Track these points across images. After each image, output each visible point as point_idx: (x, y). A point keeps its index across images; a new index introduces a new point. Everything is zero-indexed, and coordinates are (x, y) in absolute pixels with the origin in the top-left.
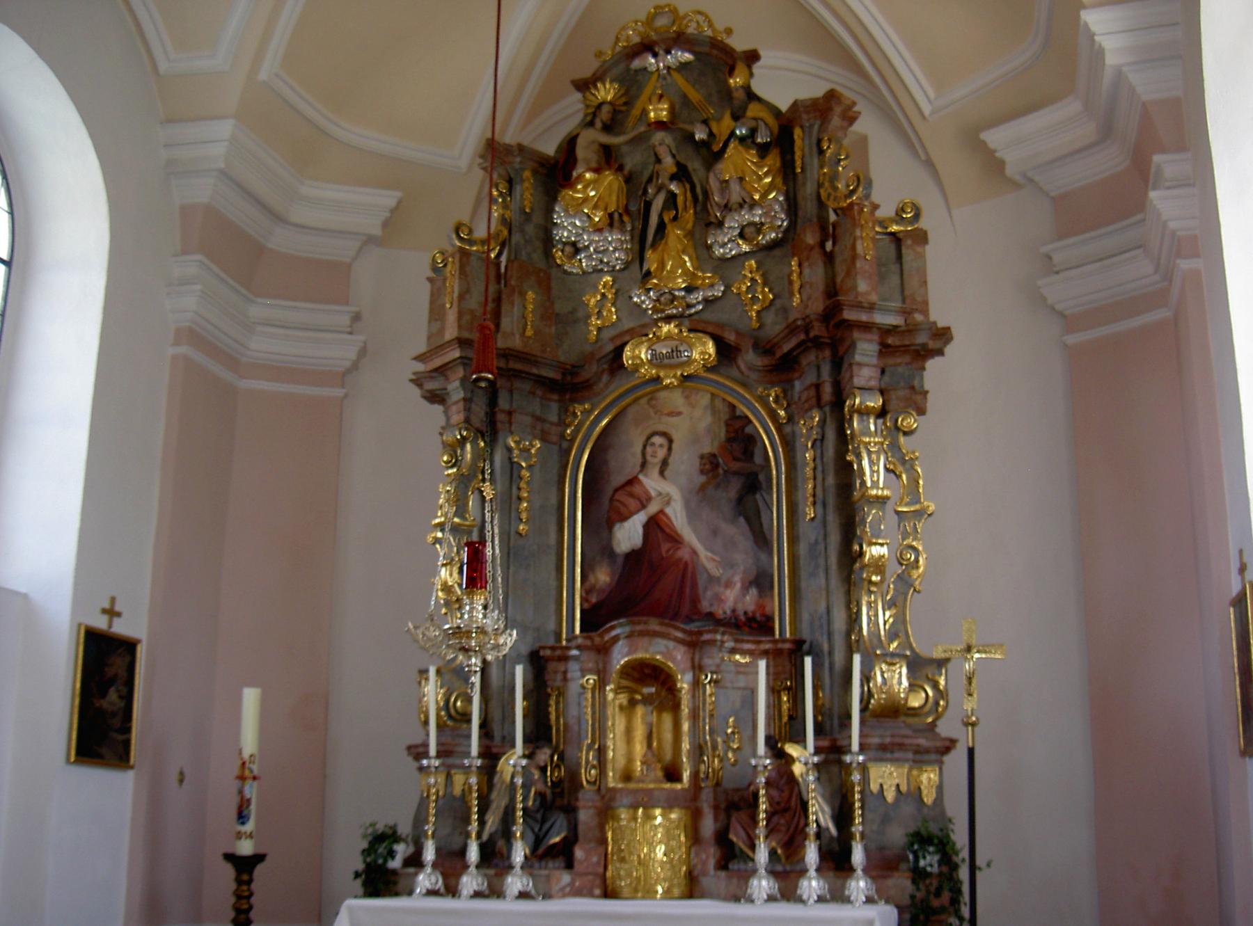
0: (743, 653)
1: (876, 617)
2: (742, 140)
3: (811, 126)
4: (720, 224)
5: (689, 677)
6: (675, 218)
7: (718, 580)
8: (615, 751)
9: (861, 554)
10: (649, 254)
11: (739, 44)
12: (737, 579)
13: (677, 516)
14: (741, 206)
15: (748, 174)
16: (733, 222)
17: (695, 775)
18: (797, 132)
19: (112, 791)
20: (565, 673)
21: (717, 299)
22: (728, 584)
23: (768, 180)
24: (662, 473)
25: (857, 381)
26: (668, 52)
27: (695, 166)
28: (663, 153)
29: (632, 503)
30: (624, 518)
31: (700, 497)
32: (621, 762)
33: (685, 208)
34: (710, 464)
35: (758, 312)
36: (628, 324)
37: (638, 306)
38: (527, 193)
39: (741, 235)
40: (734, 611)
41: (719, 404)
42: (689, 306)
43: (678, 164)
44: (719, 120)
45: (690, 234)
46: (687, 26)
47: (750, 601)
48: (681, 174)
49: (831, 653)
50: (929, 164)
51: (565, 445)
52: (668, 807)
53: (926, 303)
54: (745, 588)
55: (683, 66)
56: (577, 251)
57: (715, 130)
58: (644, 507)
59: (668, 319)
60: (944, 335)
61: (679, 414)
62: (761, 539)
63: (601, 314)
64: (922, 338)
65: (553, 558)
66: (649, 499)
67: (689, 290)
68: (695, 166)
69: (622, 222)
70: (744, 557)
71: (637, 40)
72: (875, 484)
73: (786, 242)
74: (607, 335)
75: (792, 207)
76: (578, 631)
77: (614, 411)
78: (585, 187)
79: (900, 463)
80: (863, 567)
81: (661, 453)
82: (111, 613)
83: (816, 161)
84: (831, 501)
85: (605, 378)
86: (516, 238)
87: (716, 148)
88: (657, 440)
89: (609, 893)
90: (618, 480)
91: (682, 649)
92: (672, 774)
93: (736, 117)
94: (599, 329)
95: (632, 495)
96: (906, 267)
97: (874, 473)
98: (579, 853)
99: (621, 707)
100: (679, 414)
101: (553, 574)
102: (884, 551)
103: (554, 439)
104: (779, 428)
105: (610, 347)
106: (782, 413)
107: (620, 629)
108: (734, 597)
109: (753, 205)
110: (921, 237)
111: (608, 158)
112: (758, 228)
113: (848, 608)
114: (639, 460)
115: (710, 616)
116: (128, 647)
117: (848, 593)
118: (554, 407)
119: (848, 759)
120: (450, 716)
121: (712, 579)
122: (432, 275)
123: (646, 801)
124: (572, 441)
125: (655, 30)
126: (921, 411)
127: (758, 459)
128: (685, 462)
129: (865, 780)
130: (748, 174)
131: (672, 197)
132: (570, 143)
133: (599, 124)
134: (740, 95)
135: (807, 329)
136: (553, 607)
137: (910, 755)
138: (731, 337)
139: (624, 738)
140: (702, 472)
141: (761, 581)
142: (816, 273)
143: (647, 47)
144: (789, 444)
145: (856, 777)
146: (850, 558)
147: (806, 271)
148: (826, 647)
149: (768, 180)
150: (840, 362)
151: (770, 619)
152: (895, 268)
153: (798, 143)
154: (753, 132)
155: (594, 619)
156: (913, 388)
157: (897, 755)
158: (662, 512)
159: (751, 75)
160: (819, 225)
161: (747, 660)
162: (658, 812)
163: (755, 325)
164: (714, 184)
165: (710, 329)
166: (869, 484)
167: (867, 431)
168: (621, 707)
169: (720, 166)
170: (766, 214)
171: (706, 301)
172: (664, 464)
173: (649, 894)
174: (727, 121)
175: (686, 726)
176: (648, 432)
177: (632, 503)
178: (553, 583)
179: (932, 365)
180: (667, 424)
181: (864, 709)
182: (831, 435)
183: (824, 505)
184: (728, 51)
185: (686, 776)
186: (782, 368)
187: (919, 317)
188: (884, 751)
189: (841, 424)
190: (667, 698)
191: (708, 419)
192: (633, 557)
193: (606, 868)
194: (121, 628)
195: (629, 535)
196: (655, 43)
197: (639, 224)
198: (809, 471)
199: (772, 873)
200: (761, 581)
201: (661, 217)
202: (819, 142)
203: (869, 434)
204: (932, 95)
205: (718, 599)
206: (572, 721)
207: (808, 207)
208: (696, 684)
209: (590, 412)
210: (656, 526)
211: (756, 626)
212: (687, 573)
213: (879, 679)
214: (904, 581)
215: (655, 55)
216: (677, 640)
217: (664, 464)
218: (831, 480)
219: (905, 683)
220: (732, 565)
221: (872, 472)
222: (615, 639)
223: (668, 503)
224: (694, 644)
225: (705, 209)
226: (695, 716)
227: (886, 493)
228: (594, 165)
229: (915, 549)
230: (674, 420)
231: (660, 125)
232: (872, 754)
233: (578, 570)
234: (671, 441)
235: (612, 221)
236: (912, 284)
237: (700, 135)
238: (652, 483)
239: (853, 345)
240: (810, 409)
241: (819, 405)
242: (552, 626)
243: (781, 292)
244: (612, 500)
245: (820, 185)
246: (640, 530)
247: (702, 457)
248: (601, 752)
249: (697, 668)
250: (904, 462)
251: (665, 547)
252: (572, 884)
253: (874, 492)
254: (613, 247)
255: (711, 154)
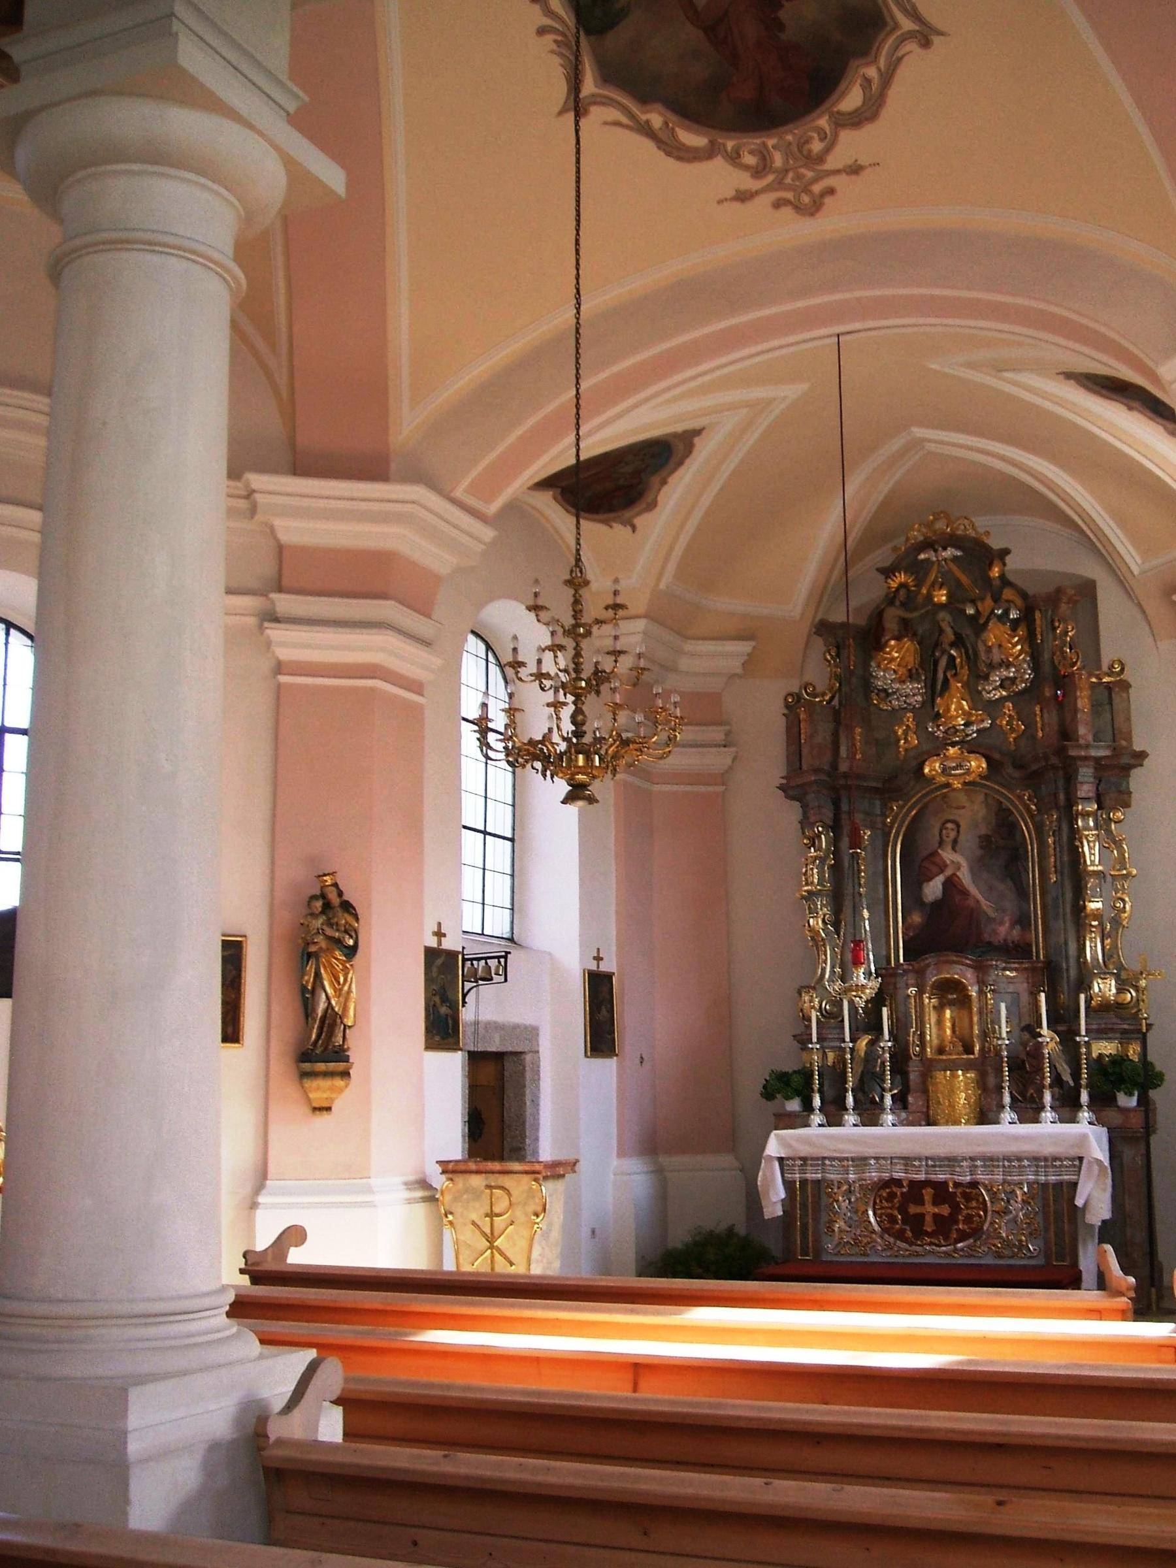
0: (1010, 970)
1: (1094, 949)
2: (1000, 617)
3: (1046, 611)
4: (986, 678)
5: (976, 988)
6: (956, 674)
7: (994, 920)
8: (931, 1034)
9: (1085, 907)
10: (938, 700)
11: (995, 543)
12: (1007, 919)
13: (965, 877)
14: (1000, 665)
15: (1005, 643)
16: (996, 678)
17: (982, 1049)
18: (1038, 615)
19: (608, 1067)
20: (895, 984)
21: (985, 729)
22: (1001, 923)
23: (1019, 647)
24: (954, 849)
25: (1081, 794)
26: (945, 549)
27: (967, 632)
28: (944, 625)
29: (935, 869)
30: (931, 879)
31: (979, 866)
32: (935, 1042)
33: (962, 667)
34: (986, 842)
35: (1015, 739)
36: (926, 747)
37: (933, 733)
38: (853, 657)
39: (1001, 686)
40: (1005, 940)
41: (990, 800)
42: (967, 735)
43: (956, 634)
44: (982, 599)
45: (966, 685)
46: (957, 529)
47: (1016, 933)
48: (958, 642)
49: (1068, 970)
50: (1140, 605)
51: (887, 830)
52: (966, 1070)
53: (1130, 733)
54: (1012, 926)
55: (955, 559)
56: (888, 695)
57: (980, 609)
58: (942, 871)
59: (953, 744)
60: (1141, 756)
61: (964, 807)
62: (1023, 893)
63: (907, 739)
64: (1125, 760)
65: (882, 907)
66: (946, 866)
67: (967, 725)
68: (967, 632)
69: (918, 674)
70: (1011, 904)
71: (921, 538)
72: (1092, 862)
73: (1033, 689)
74: (912, 754)
75: (1036, 666)
76: (901, 961)
77: (919, 806)
78: (892, 650)
79: (1111, 841)
80: (1086, 916)
81: (953, 834)
82: (598, 959)
83: (1051, 635)
84: (1066, 871)
85: (912, 783)
86: (845, 689)
87: (982, 621)
88: (949, 825)
89: (930, 1123)
90: (925, 853)
91: (970, 970)
92: (969, 1049)
93: (996, 600)
94: (906, 750)
95: (934, 863)
96: (1115, 707)
97: (1092, 855)
98: (910, 1099)
99: (934, 1007)
100: (964, 807)
101: (882, 915)
102: (1099, 905)
103: (880, 826)
104: (1032, 816)
105: (914, 763)
106: (1033, 807)
107: (930, 959)
108: (1004, 931)
109: (1008, 665)
110: (1125, 686)
111: (906, 629)
112: (1013, 680)
113: (1078, 941)
114: (938, 838)
115: (990, 943)
116: (609, 977)
117: (1078, 931)
118: (878, 803)
119: (1078, 1039)
120: (822, 1014)
121: (991, 920)
122: (786, 712)
123: (953, 1066)
124: (891, 828)
125: (935, 532)
126: (1126, 805)
127: (1018, 837)
128: (968, 840)
129: (1089, 1053)
130: (1005, 643)
131: (953, 658)
132: (878, 616)
133: (898, 603)
134: (997, 583)
135: (1046, 758)
136: (883, 940)
137: (1118, 1035)
138: (996, 756)
139: (937, 1026)
140: (981, 847)
141: (1023, 921)
142: (1052, 718)
143: (928, 545)
144: (1039, 828)
145: (1084, 1050)
146: (1079, 909)
147: (1046, 715)
148: (1064, 965)
149: (1019, 647)
150: (1070, 780)
151: (1030, 945)
152: (1107, 707)
153: (1038, 622)
154: (1006, 612)
155: (913, 950)
156: (1120, 792)
157: (1110, 1035)
158: (954, 874)
159: (1004, 564)
160: (1051, 682)
161: (1014, 974)
162: (960, 1072)
163: (1013, 748)
164: (981, 648)
165: (982, 751)
166: (1088, 863)
167: (1087, 825)
168: (934, 1007)
169: (984, 635)
170: (1017, 671)
171: (978, 731)
172: (955, 841)
173: (957, 1122)
174: (989, 602)
175: (975, 1019)
176: (943, 820)
177: (935, 869)
178: (883, 922)
179: (1135, 773)
180: (955, 814)
181: (1088, 1008)
182: (1065, 827)
183: (1062, 875)
184: (987, 549)
185: (977, 1048)
186: (1033, 779)
187: (1124, 743)
188: (1098, 1033)
189: (1072, 820)
190: (964, 1001)
191: (982, 812)
192: (937, 905)
193: (928, 1107)
194: (604, 967)
195: (933, 889)
196: (935, 542)
197: (931, 674)
198: (1052, 852)
199: (1090, 1107)
200: (1023, 921)
201: (945, 673)
202: (1053, 621)
203: (1089, 829)
204: (1139, 561)
205: (995, 932)
206: (900, 1015)
207: (1047, 668)
208: (981, 992)
209: (903, 807)
210: (951, 884)
211: (1017, 952)
212: (974, 916)
213: (1096, 990)
214: (1116, 922)
215: (936, 551)
216: (968, 966)
217: (955, 841)
218: (1066, 858)
219: (1114, 991)
220: (1003, 910)
221: (1091, 854)
222: (928, 965)
223: (959, 869)
224: (981, 969)
225: (976, 665)
226: (980, 1012)
227: (1100, 868)
228: (896, 633)
229: (1123, 900)
230: (962, 812)
231: (942, 606)
232: (1093, 1035)
233: (900, 914)
234: (958, 826)
235: (912, 676)
236: (1120, 719)
237: (970, 611)
238: (947, 855)
239: (1076, 771)
240: (1051, 809)
241: (1057, 807)
242: (884, 953)
243: (1030, 726)
244: (920, 867)
245: (1054, 654)
246: (940, 887)
247: (980, 837)
248: (922, 1037)
249: (982, 983)
250: (1115, 842)
251: (958, 898)
252: (906, 1119)
253: (1091, 868)
254: (914, 692)
255: (978, 625)
